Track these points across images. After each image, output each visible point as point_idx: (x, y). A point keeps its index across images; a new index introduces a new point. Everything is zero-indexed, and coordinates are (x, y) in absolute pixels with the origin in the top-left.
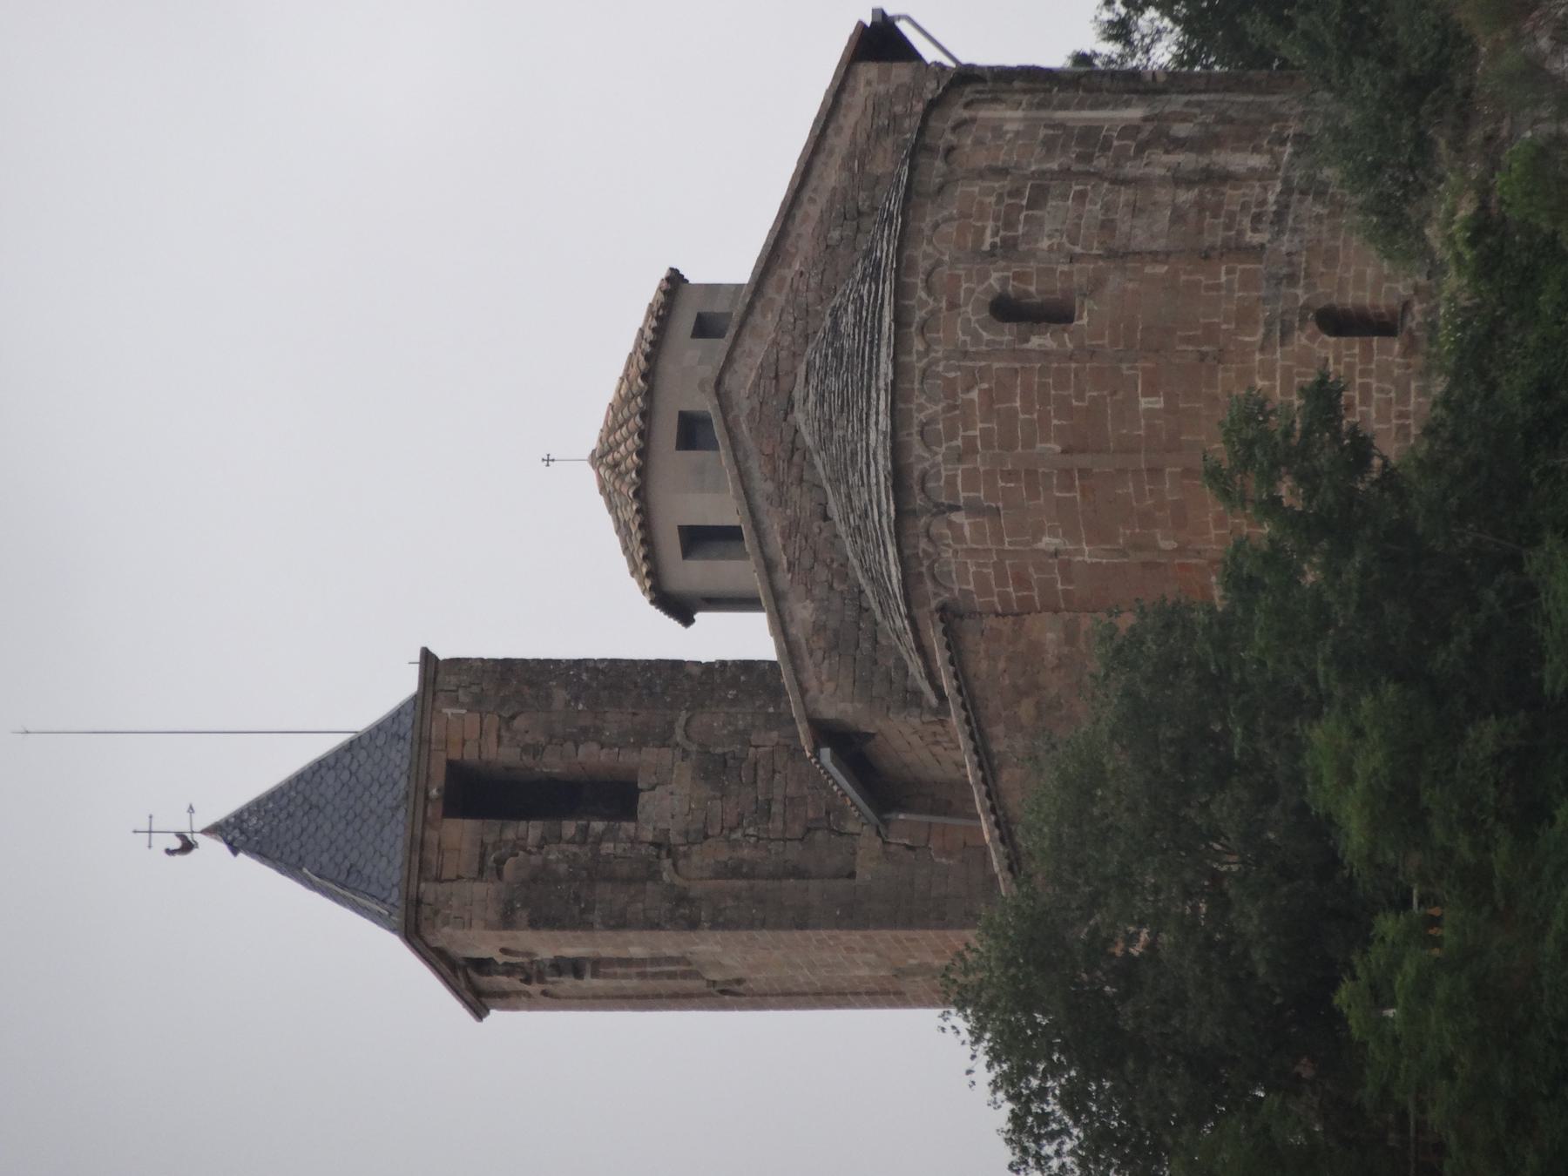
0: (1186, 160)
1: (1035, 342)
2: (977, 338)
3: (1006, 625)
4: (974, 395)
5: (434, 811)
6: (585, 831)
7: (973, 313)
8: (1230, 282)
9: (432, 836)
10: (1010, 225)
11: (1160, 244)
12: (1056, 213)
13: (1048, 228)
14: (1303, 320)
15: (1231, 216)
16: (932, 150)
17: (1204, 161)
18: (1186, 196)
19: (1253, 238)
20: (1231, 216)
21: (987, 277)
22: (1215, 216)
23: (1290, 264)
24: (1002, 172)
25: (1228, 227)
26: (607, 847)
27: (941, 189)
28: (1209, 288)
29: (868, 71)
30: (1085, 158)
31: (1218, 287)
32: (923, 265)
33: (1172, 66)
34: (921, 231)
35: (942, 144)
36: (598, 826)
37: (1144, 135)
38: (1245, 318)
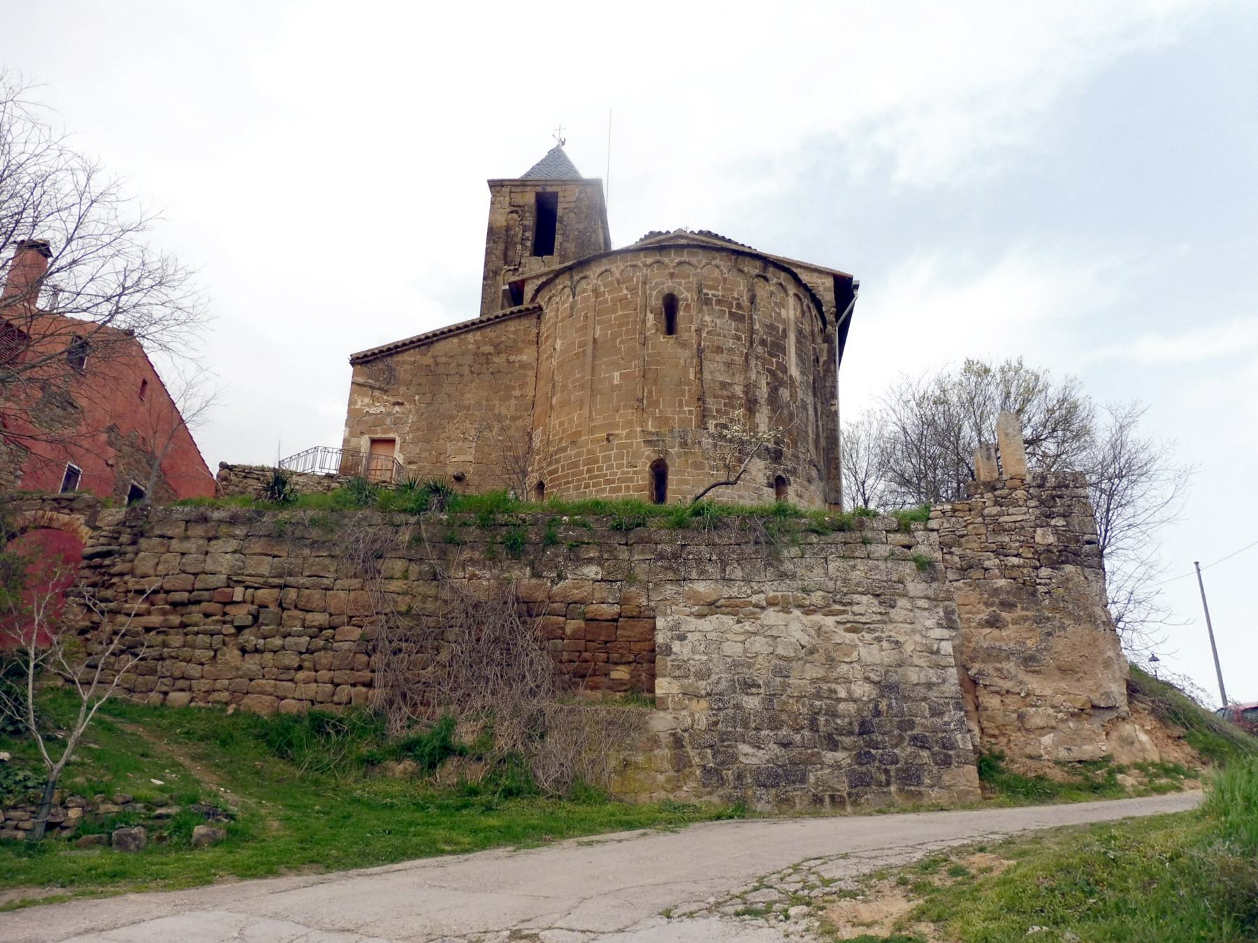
0: (763, 391)
1: (650, 316)
2: (652, 289)
3: (532, 337)
4: (625, 292)
5: (539, 189)
6: (527, 239)
7: (668, 286)
8: (684, 412)
9: (528, 189)
10: (719, 302)
11: (707, 376)
12: (727, 325)
13: (718, 321)
14: (660, 452)
15: (727, 413)
16: (765, 269)
17: (763, 401)
18: (739, 390)
19: (711, 425)
20: (727, 413)
21: (688, 291)
22: (725, 405)
23: (694, 443)
24: (752, 300)
25: (718, 411)
26: (519, 247)
27: (741, 271)
28: (680, 401)
29: (829, 282)
30: (763, 343)
31: (681, 406)
32: (694, 260)
33: (1223, 852)
34: (714, 258)
35: (769, 275)
36: (529, 244)
37: (780, 375)
38: (662, 421)
